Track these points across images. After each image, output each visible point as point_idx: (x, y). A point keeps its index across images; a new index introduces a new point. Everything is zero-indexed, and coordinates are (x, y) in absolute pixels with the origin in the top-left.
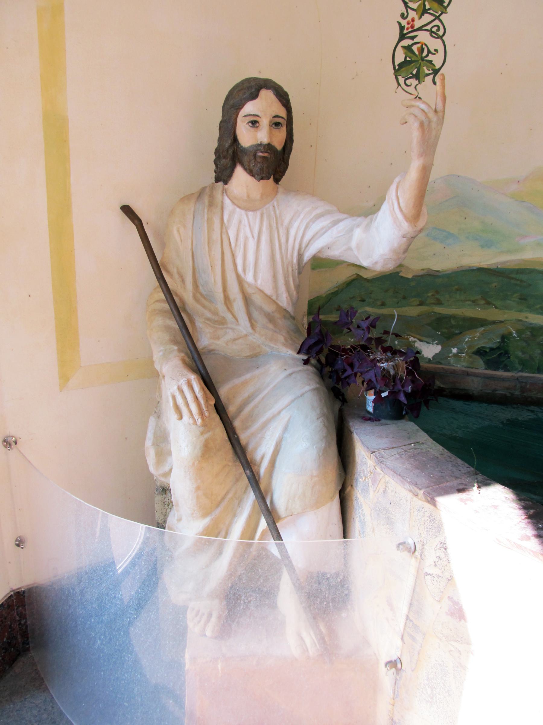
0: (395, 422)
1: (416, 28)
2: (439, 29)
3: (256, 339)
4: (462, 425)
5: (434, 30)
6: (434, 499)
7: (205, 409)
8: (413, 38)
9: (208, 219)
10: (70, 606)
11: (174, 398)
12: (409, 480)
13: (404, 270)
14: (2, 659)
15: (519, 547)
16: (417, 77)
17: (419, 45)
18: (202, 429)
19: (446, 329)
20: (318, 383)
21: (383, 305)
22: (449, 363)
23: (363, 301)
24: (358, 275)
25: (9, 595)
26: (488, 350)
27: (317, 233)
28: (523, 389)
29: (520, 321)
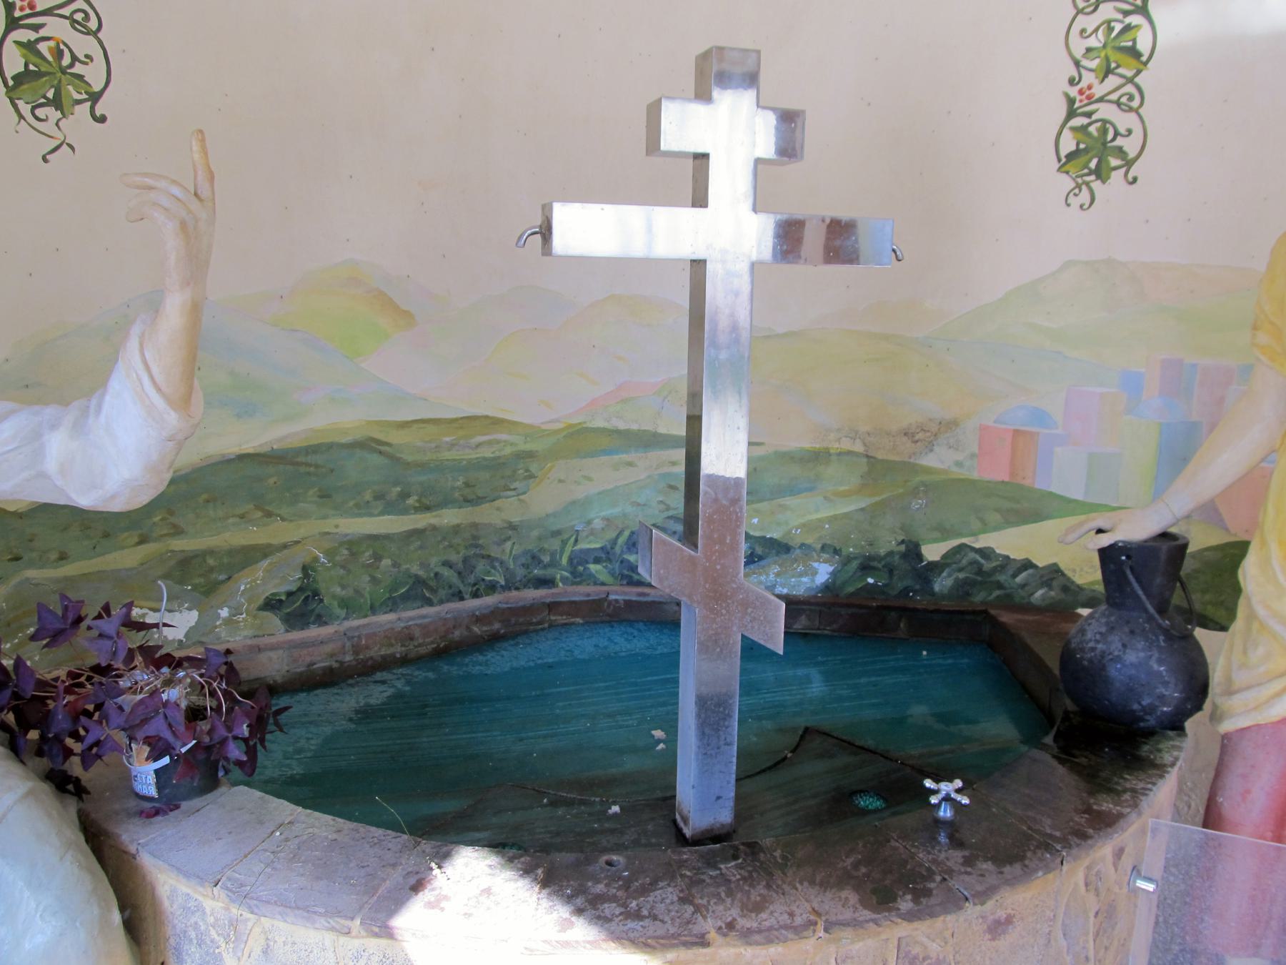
0: (210, 797)
1: (39, 9)
2: (87, 17)
4: (290, 749)
5: (79, 16)
6: (387, 927)
8: (36, 28)
10: (1034, 853)
12: (322, 910)
15: (566, 944)
16: (57, 102)
17: (52, 44)
19: (200, 577)
21: (63, 557)
22: (219, 639)
23: (17, 559)
26: (283, 598)
28: (357, 650)
29: (328, 533)
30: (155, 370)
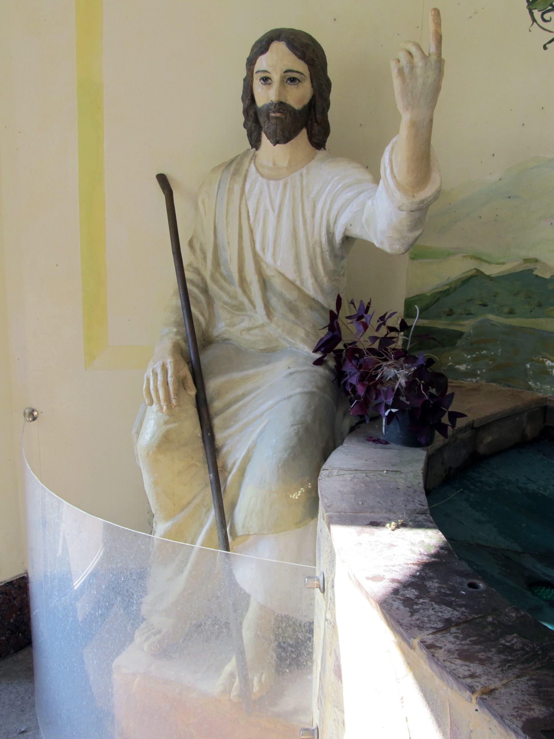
3: (274, 330)
7: (173, 397)
9: (229, 189)
11: (148, 380)
13: (538, 267)
14: (7, 640)
15: (359, 585)
18: (167, 418)
20: (318, 387)
21: (511, 312)
23: (485, 305)
24: (478, 270)
25: (22, 576)
27: (342, 207)
30: (395, 171)
